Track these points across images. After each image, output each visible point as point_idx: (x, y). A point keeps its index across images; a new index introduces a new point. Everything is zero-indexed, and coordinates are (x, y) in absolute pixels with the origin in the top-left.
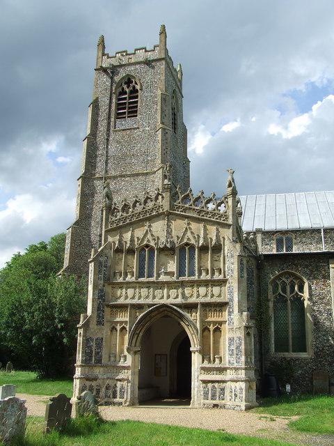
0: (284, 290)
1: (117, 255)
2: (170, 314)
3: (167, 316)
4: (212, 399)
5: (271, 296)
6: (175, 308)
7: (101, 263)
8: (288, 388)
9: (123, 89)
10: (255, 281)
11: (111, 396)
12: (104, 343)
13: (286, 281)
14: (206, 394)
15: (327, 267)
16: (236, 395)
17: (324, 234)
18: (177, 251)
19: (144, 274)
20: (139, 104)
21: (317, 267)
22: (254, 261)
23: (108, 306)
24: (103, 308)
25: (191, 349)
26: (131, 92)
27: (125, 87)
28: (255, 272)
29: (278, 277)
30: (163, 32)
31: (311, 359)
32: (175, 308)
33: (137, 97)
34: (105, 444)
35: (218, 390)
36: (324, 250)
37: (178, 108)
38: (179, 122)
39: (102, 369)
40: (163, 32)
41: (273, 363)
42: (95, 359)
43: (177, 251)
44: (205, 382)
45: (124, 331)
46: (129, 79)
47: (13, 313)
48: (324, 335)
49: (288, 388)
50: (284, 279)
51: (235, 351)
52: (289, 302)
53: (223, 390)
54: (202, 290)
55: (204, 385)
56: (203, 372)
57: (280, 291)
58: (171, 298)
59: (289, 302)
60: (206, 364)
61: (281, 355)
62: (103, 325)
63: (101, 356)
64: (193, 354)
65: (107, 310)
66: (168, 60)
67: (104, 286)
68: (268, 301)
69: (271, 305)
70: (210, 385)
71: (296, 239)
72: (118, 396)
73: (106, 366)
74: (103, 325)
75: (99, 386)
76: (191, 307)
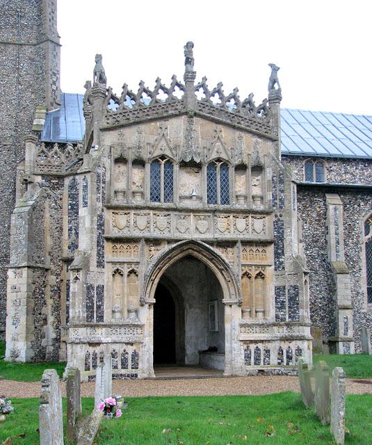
1: (117, 166)
2: (196, 254)
3: (190, 258)
4: (255, 364)
11: (120, 366)
12: (105, 293)
14: (248, 357)
18: (205, 169)
21: (311, 202)
23: (108, 239)
24: (103, 242)
25: (224, 301)
34: (189, 443)
35: (262, 352)
43: (205, 169)
44: (245, 342)
47: (324, 250)
51: (287, 304)
53: (268, 351)
54: (241, 223)
55: (245, 346)
56: (243, 329)
58: (194, 229)
60: (248, 320)
62: (103, 267)
64: (227, 309)
65: (108, 246)
70: (252, 347)
72: (130, 366)
73: (109, 326)
76: (228, 244)
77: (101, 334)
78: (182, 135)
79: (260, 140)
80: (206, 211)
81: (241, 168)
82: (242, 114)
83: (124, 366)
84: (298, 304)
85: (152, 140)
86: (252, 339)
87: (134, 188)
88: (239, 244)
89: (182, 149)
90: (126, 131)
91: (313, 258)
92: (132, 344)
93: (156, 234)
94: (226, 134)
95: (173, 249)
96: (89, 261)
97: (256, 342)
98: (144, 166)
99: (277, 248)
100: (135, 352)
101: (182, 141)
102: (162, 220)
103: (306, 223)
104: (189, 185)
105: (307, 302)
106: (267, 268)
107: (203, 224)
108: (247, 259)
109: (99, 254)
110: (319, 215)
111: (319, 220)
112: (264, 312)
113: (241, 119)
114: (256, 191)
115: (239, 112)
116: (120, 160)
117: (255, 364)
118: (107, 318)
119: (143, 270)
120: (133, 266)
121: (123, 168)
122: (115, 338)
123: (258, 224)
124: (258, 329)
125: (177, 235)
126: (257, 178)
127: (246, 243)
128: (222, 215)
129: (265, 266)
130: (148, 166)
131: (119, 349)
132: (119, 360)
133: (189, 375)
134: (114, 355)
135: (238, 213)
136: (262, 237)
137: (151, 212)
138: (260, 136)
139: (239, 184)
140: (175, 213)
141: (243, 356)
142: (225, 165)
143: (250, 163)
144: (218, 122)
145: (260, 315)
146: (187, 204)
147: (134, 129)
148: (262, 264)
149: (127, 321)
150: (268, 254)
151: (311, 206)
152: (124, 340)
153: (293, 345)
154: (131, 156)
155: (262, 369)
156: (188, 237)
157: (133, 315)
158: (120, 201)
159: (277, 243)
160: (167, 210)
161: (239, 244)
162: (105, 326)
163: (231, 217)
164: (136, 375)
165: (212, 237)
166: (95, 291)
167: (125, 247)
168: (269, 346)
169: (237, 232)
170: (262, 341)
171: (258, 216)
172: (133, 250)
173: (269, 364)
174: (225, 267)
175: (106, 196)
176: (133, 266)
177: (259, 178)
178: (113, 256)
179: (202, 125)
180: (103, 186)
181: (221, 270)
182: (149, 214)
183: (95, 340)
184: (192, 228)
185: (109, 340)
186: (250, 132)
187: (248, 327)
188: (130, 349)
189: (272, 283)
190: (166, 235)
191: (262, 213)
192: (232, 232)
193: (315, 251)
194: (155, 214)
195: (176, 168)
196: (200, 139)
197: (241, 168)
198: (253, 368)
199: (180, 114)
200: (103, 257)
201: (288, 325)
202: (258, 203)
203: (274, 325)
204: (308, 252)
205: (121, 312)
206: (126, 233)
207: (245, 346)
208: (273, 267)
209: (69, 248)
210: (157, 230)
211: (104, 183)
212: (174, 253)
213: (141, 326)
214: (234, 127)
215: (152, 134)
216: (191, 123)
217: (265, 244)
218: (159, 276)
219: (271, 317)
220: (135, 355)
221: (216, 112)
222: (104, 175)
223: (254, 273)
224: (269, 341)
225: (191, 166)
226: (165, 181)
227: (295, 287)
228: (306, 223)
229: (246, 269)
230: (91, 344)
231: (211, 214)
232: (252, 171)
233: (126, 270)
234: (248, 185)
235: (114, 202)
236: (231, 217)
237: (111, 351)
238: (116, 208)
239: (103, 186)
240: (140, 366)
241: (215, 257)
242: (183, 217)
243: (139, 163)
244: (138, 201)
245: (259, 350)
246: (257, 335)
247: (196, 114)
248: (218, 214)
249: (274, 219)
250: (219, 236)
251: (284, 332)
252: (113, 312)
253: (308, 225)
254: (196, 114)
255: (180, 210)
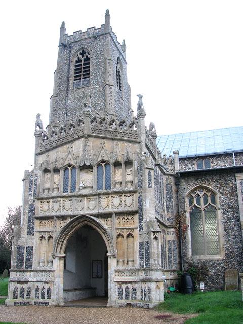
0: (199, 203)
1: (46, 174)
4: (125, 299)
5: (188, 208)
6: (93, 217)
7: (31, 181)
8: (202, 285)
9: (79, 58)
10: (174, 196)
11: (40, 297)
12: (34, 251)
13: (200, 194)
14: (120, 293)
15: (234, 180)
16: (145, 295)
17: (235, 158)
18: (95, 168)
19: (67, 190)
20: (91, 69)
22: (172, 179)
23: (37, 218)
25: (108, 254)
26: (85, 60)
27: (81, 56)
28: (174, 188)
29: (193, 191)
30: (107, 15)
31: (223, 260)
32: (93, 217)
33: (89, 63)
35: (131, 290)
36: (228, 166)
37: (122, 72)
38: (123, 82)
39: (32, 273)
40: (107, 15)
41: (191, 265)
42: (26, 265)
44: (118, 282)
45: (43, 240)
46: (83, 51)
48: (233, 239)
49: (202, 285)
50: (198, 192)
51: (144, 255)
52: (203, 212)
53: (134, 290)
54: (117, 201)
55: (119, 286)
56: (117, 274)
57: (195, 203)
58: (86, 208)
59: (203, 212)
60: (121, 267)
61: (196, 258)
62: (33, 235)
63: (32, 263)
64: (109, 259)
65: (37, 222)
66: (112, 35)
67: (34, 201)
68: (185, 212)
69: (188, 215)
70: (124, 286)
71: (212, 162)
72: (46, 297)
73: (36, 271)
74: (33, 235)
75: (30, 288)
76: (106, 216)
77: (29, 276)
78: (81, 150)
79: (130, 144)
80: (94, 195)
81: (117, 164)
82: (119, 130)
83: (43, 297)
84: (149, 255)
85: (64, 155)
86: (122, 280)
87: (55, 186)
88: (114, 215)
89: (80, 158)
90: (51, 153)
91: (230, 219)
92: (48, 283)
93: (64, 213)
94: (108, 144)
95: (72, 222)
96: (20, 232)
97: (126, 283)
98: (59, 171)
99: (140, 216)
100: (49, 288)
101: (81, 153)
102: (67, 204)
103: (223, 195)
104: (87, 179)
105: (158, 254)
106: (135, 230)
107: (92, 204)
108: (120, 225)
109: (29, 227)
110: (232, 189)
111: (232, 193)
112: (133, 261)
113: (118, 133)
114: (129, 178)
115: (117, 129)
116: (46, 171)
117: (125, 299)
118: (35, 266)
119: (55, 235)
120: (120, 231)
121: (49, 175)
122: (38, 279)
123: (128, 200)
124: (128, 274)
125: (76, 213)
126: (130, 169)
127: (119, 214)
128: (104, 197)
129: (133, 229)
130: (62, 172)
131: (40, 285)
132: (40, 292)
133: (94, 304)
134: (37, 290)
135: (115, 194)
136: (130, 209)
137: (62, 200)
138: (130, 142)
139: (118, 175)
140: (75, 198)
141: (117, 293)
142: (107, 163)
143: (121, 160)
144: (103, 138)
145: (130, 263)
146: (84, 192)
147: (55, 151)
148: (131, 227)
149: (46, 268)
150: (135, 220)
151: (225, 183)
152: (43, 280)
153: (147, 285)
154: (51, 167)
155: (130, 302)
156: (82, 213)
157: (50, 264)
158: (45, 195)
159: (137, 212)
160: (70, 197)
161: (114, 215)
162: (33, 271)
163: (123, 196)
164: (48, 303)
165: (97, 212)
166: (25, 250)
167: (47, 222)
168: (136, 286)
169: (114, 207)
170: (130, 282)
171: (128, 195)
172: (50, 224)
173: (135, 299)
174: (105, 232)
175: (37, 193)
176: (120, 231)
177: (131, 169)
178: (40, 228)
179: (93, 142)
180: (35, 187)
181: (104, 233)
182: (60, 201)
183: (24, 280)
184: (85, 207)
185: (35, 280)
186: (123, 140)
187: (121, 272)
188: (47, 286)
189: (137, 240)
190: (70, 213)
191: (130, 192)
192: (110, 207)
193: (230, 215)
194: (64, 201)
195: (112, 167)
196: (92, 150)
197: (117, 164)
198: (124, 301)
199: (79, 138)
200: (34, 229)
201: (145, 271)
202: (129, 186)
203: (139, 270)
204: (225, 216)
205: (44, 262)
206: (48, 214)
207: (119, 286)
208: (138, 229)
209: (167, 219)
210: (65, 210)
211: (36, 185)
212: (75, 224)
213: (53, 272)
214: (113, 139)
215: (64, 152)
216: (86, 141)
217: (133, 213)
218: (67, 239)
219: (137, 266)
220: (49, 290)
221: (103, 132)
222: (36, 180)
223: (125, 234)
224: (135, 282)
225: (85, 168)
226: (106, 179)
227: (148, 243)
228: (223, 195)
229: (120, 232)
230: (19, 282)
231: (97, 197)
232: (126, 165)
233: (46, 237)
234: (123, 175)
235: (41, 196)
236: (123, 196)
237: (36, 287)
238: (42, 199)
239: (35, 187)
240: (52, 297)
241: (99, 225)
242: (80, 200)
243: (56, 171)
244: (55, 194)
245: (128, 288)
246: (123, 278)
247: (89, 136)
248: (101, 196)
249: (139, 195)
250: (101, 211)
251: (141, 275)
252: (39, 263)
253: (224, 197)
254: (89, 136)
255: (78, 196)
